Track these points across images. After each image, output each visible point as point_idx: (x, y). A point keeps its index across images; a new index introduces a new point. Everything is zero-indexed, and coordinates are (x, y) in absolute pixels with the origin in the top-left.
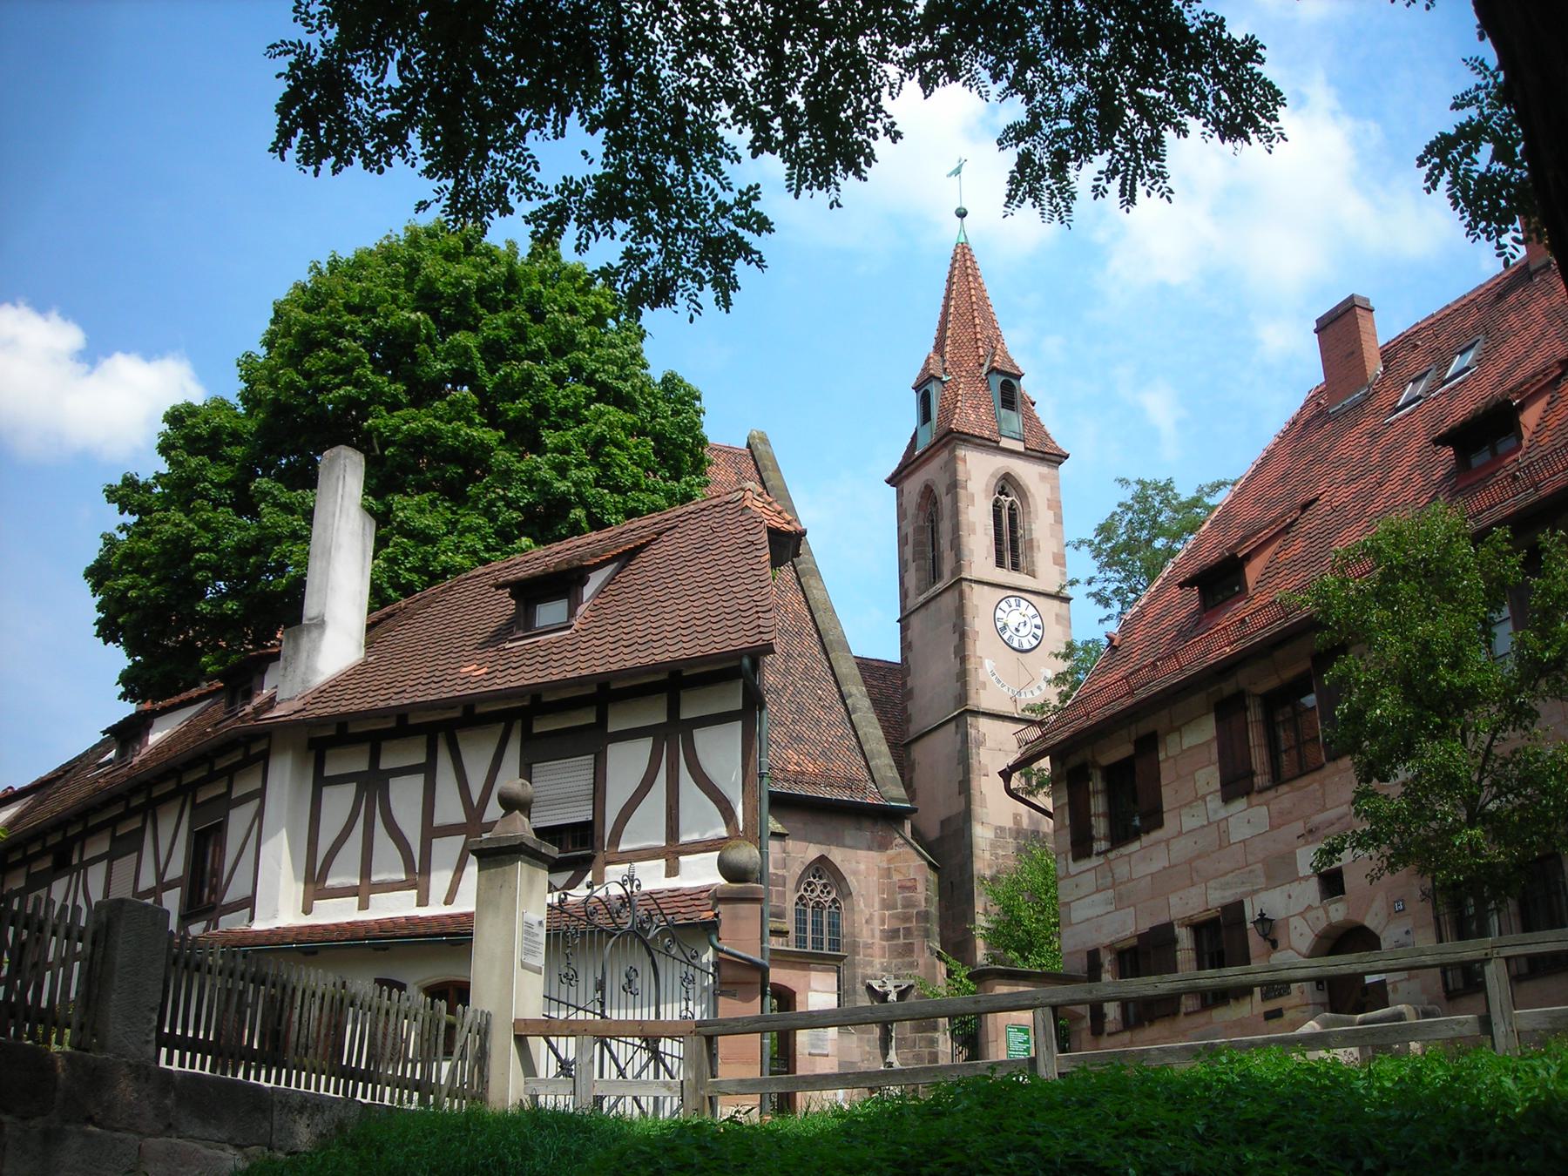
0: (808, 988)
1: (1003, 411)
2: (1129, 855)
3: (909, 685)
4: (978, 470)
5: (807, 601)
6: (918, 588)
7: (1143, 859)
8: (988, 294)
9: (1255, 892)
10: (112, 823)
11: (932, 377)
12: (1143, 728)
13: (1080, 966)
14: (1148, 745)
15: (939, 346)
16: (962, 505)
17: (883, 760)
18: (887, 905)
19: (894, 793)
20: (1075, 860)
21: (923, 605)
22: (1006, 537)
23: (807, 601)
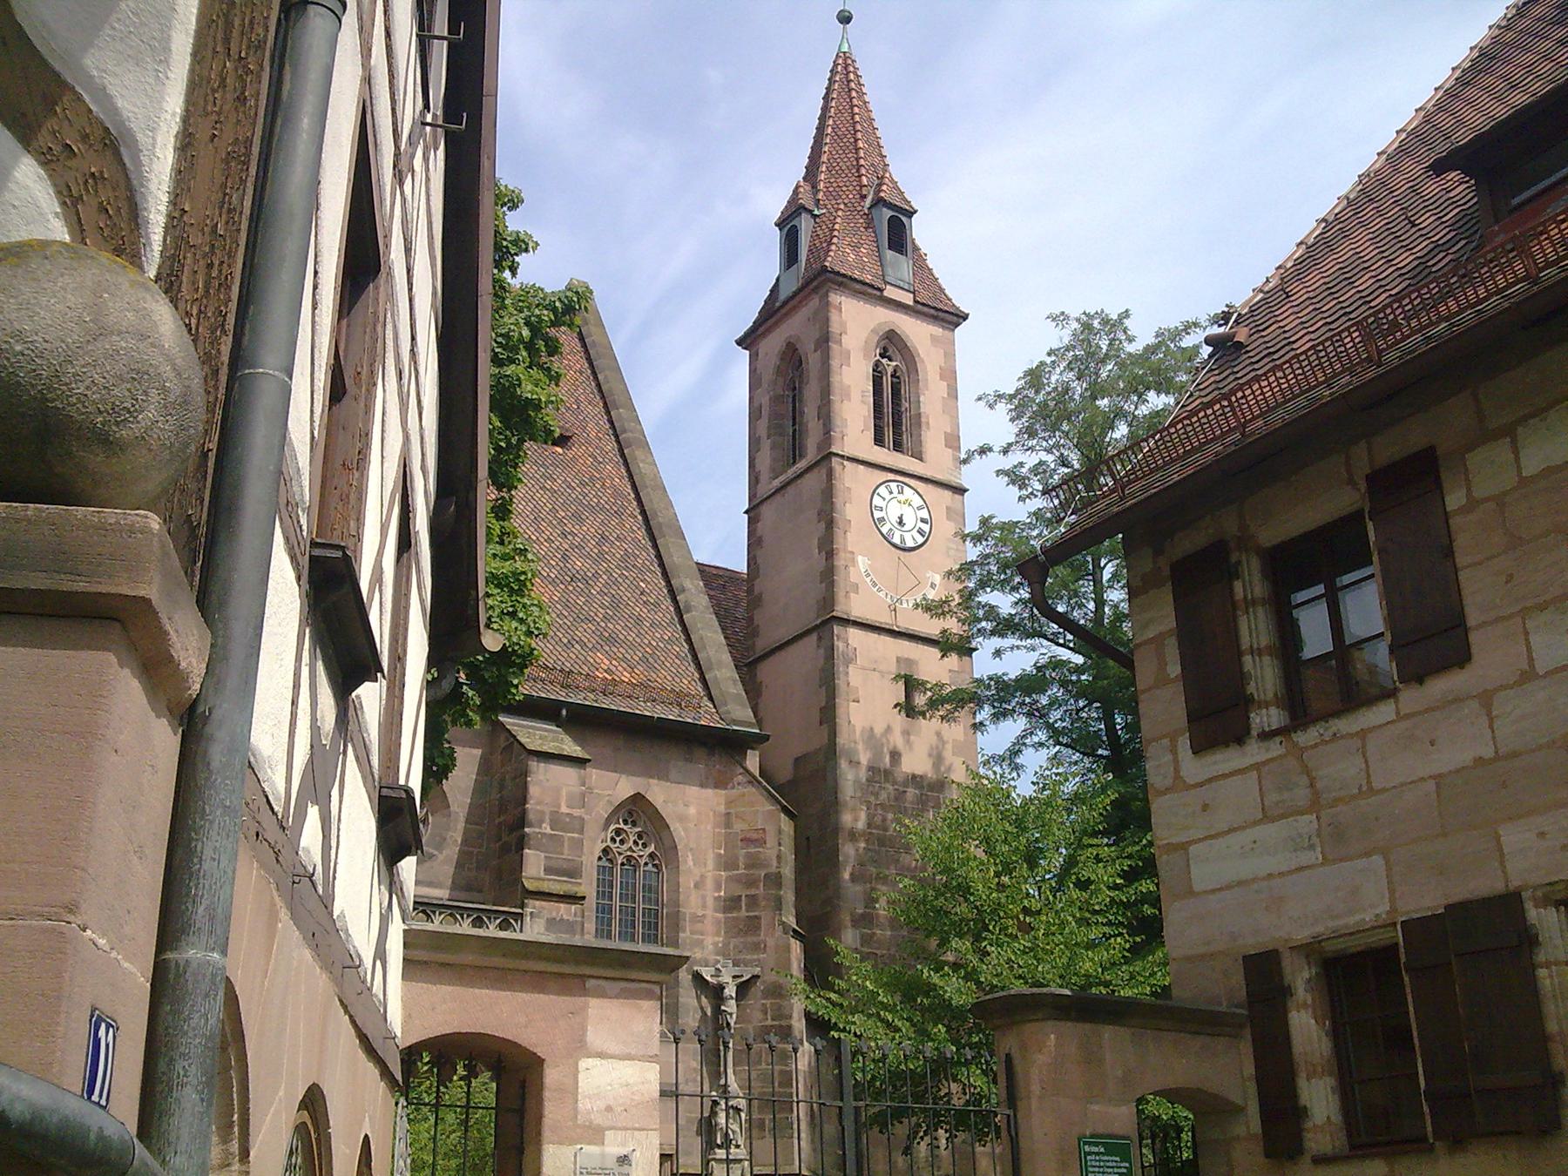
0: (579, 1047)
1: (890, 255)
2: (1363, 734)
4: (856, 324)
5: (631, 477)
6: (773, 470)
8: (873, 115)
12: (1392, 446)
13: (1226, 988)
14: (1413, 481)
15: (811, 174)
16: (835, 363)
17: (725, 673)
18: (728, 863)
19: (739, 715)
20: (1198, 749)
21: (778, 491)
22: (888, 409)
23: (631, 477)
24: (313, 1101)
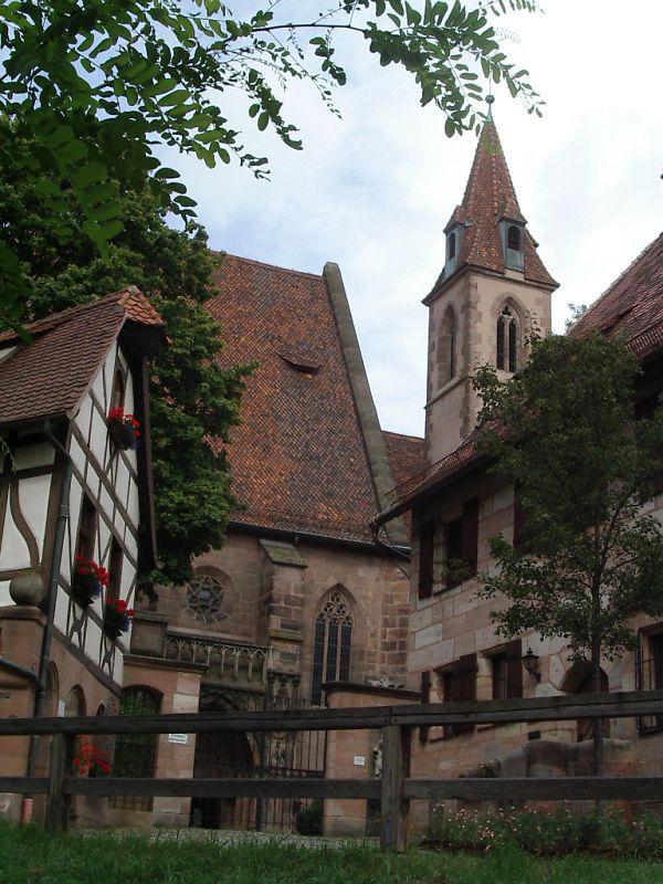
0: (174, 691)
3: (429, 457)
16: (472, 321)
20: (420, 598)
24: (78, 690)
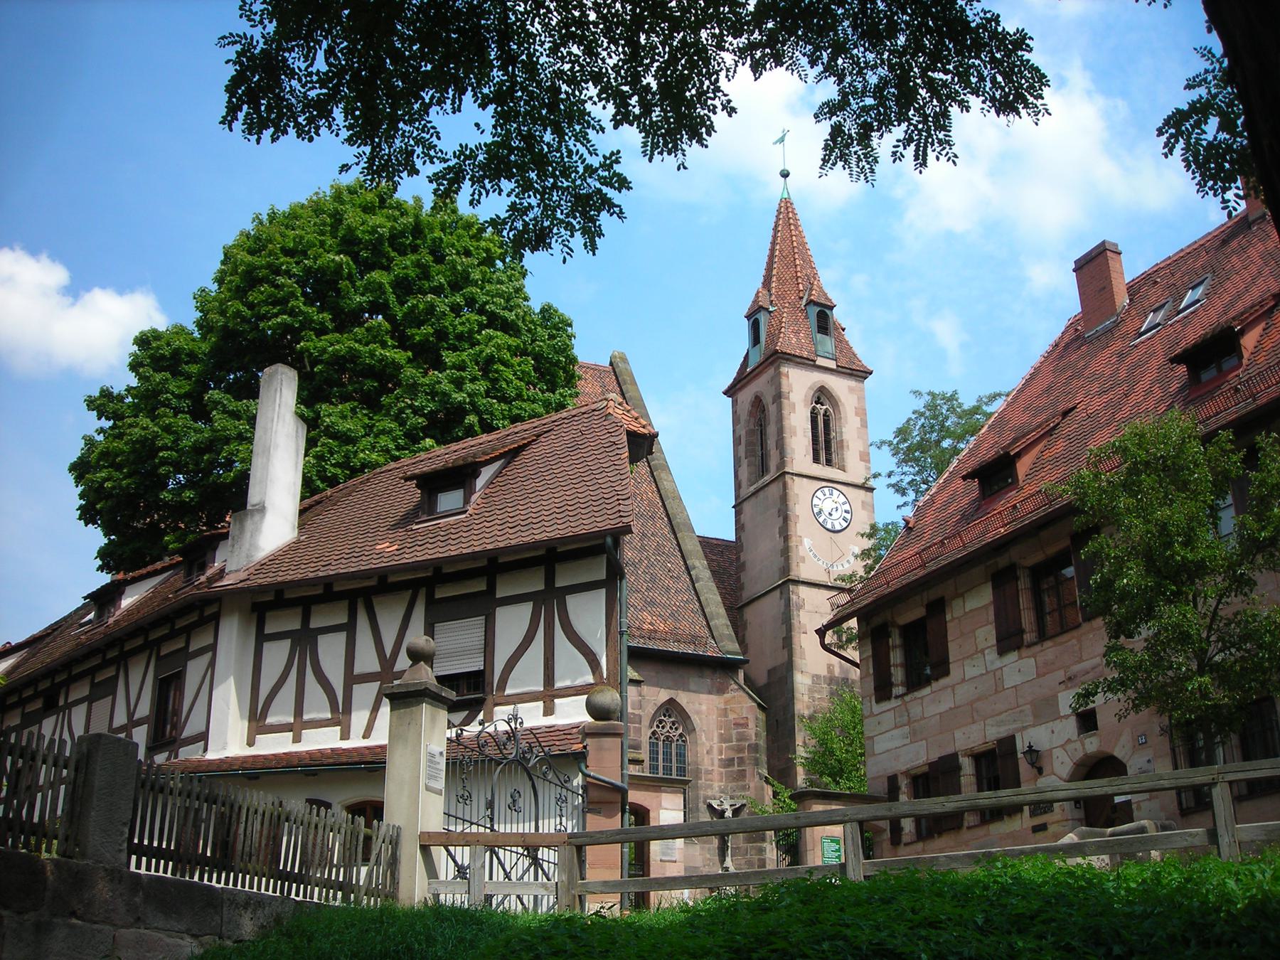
0: (660, 806)
1: (819, 336)
2: (922, 698)
3: (742, 559)
4: (798, 384)
5: (659, 491)
6: (749, 480)
7: (933, 701)
8: (806, 240)
9: (1024, 728)
10: (92, 672)
11: (761, 308)
12: (933, 594)
13: (881, 788)
14: (938, 608)
15: (767, 283)
16: (785, 412)
17: (721, 620)
18: (724, 739)
19: (730, 648)
20: (877, 702)
21: (754, 494)
22: (822, 438)
23: (659, 491)
